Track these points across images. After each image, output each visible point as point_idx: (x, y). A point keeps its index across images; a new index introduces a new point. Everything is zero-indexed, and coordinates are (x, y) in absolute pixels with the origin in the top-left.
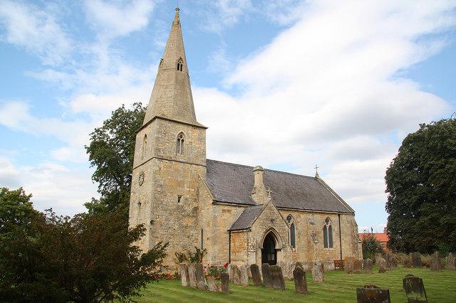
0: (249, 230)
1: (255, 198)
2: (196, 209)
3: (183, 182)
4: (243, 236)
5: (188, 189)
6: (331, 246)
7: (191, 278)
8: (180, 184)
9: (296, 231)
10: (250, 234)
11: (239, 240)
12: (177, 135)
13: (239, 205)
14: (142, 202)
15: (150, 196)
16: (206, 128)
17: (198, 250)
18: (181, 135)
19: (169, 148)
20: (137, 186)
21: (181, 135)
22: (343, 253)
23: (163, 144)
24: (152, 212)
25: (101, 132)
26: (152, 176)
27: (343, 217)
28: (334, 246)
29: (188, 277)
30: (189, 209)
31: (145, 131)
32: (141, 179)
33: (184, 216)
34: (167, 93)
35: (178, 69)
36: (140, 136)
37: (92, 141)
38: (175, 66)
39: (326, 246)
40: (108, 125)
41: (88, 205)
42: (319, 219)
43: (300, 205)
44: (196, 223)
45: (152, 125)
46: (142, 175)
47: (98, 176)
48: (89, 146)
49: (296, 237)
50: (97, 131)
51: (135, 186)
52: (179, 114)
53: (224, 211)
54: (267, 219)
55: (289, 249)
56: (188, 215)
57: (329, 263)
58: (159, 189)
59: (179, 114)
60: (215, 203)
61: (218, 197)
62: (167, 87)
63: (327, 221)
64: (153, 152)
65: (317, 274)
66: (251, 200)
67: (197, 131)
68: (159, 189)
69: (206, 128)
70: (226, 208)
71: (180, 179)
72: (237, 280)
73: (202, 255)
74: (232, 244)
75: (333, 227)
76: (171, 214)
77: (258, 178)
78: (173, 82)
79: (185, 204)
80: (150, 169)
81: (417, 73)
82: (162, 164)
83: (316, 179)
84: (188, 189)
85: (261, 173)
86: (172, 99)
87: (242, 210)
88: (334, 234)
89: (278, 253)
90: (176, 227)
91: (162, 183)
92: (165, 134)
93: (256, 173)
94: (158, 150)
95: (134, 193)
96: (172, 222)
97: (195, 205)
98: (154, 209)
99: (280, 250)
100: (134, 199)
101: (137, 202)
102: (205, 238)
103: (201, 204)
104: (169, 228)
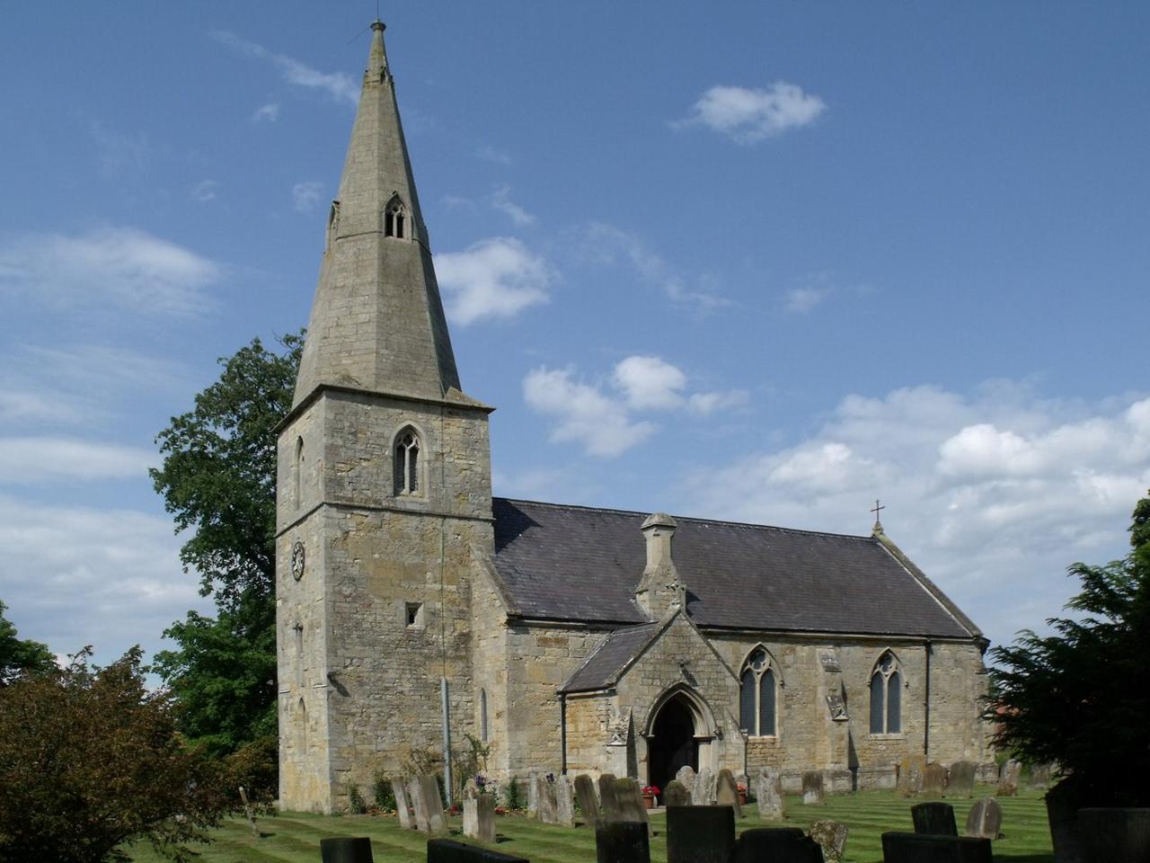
0: (611, 691)
1: (644, 603)
2: (466, 638)
3: (421, 569)
4: (598, 705)
5: (438, 586)
6: (894, 727)
7: (417, 809)
8: (414, 573)
9: (778, 691)
10: (614, 700)
11: (585, 714)
12: (392, 433)
13: (593, 626)
14: (305, 623)
15: (321, 607)
16: (489, 411)
17: (475, 744)
18: (407, 435)
19: (374, 474)
20: (291, 579)
21: (407, 435)
22: (931, 745)
23: (351, 463)
24: (332, 651)
25: (192, 427)
26: (322, 553)
27: (942, 650)
28: (903, 728)
29: (410, 805)
30: (445, 639)
31: (300, 427)
32: (298, 565)
33: (428, 657)
34: (356, 309)
35: (389, 232)
36: (287, 440)
37: (168, 454)
38: (375, 222)
39: (875, 727)
40: (210, 404)
41: (178, 632)
42: (859, 660)
43: (793, 621)
44: (468, 674)
45: (313, 410)
46: (300, 551)
47: (195, 552)
48: (161, 469)
49: (778, 708)
50: (178, 423)
51: (284, 582)
52: (396, 372)
53: (544, 642)
54: (666, 662)
55: (734, 737)
56: (443, 656)
57: (883, 773)
58: (347, 590)
59: (396, 372)
60: (517, 622)
61: (523, 605)
62: (353, 293)
63: (884, 660)
64: (321, 487)
65: (768, 799)
66: (634, 609)
67: (458, 425)
68: (347, 590)
69: (489, 411)
70: (550, 634)
71: (409, 560)
72: (548, 812)
73: (485, 754)
74: (569, 727)
75: (904, 678)
76: (388, 654)
77: (656, 548)
78: (372, 274)
79: (430, 624)
80: (315, 535)
81: (184, 521)
82: (351, 521)
83: (872, 542)
84: (438, 586)
85: (666, 534)
86: (372, 328)
87: (600, 638)
88: (904, 696)
89: (703, 748)
90: (407, 687)
91: (355, 571)
92: (354, 434)
93: (649, 534)
94: (333, 482)
95: (285, 601)
96: (392, 674)
97: (461, 627)
98: (335, 644)
99: (708, 740)
100: (284, 614)
101: (292, 624)
102: (491, 714)
103: (477, 626)
104: (387, 689)
